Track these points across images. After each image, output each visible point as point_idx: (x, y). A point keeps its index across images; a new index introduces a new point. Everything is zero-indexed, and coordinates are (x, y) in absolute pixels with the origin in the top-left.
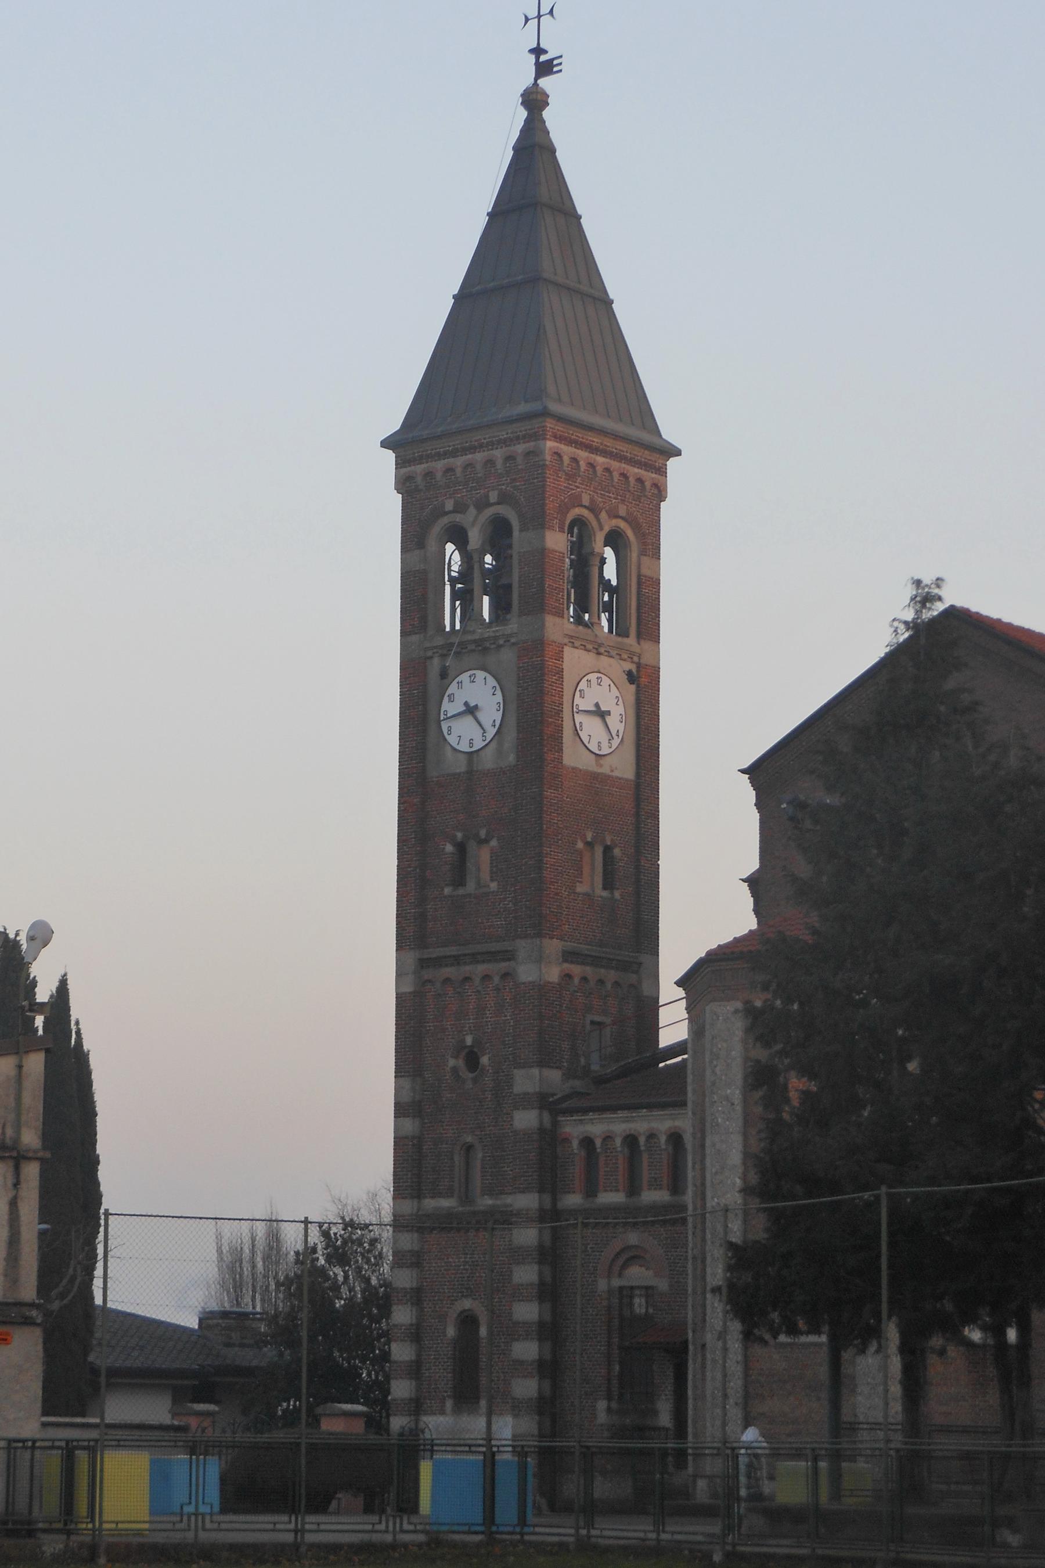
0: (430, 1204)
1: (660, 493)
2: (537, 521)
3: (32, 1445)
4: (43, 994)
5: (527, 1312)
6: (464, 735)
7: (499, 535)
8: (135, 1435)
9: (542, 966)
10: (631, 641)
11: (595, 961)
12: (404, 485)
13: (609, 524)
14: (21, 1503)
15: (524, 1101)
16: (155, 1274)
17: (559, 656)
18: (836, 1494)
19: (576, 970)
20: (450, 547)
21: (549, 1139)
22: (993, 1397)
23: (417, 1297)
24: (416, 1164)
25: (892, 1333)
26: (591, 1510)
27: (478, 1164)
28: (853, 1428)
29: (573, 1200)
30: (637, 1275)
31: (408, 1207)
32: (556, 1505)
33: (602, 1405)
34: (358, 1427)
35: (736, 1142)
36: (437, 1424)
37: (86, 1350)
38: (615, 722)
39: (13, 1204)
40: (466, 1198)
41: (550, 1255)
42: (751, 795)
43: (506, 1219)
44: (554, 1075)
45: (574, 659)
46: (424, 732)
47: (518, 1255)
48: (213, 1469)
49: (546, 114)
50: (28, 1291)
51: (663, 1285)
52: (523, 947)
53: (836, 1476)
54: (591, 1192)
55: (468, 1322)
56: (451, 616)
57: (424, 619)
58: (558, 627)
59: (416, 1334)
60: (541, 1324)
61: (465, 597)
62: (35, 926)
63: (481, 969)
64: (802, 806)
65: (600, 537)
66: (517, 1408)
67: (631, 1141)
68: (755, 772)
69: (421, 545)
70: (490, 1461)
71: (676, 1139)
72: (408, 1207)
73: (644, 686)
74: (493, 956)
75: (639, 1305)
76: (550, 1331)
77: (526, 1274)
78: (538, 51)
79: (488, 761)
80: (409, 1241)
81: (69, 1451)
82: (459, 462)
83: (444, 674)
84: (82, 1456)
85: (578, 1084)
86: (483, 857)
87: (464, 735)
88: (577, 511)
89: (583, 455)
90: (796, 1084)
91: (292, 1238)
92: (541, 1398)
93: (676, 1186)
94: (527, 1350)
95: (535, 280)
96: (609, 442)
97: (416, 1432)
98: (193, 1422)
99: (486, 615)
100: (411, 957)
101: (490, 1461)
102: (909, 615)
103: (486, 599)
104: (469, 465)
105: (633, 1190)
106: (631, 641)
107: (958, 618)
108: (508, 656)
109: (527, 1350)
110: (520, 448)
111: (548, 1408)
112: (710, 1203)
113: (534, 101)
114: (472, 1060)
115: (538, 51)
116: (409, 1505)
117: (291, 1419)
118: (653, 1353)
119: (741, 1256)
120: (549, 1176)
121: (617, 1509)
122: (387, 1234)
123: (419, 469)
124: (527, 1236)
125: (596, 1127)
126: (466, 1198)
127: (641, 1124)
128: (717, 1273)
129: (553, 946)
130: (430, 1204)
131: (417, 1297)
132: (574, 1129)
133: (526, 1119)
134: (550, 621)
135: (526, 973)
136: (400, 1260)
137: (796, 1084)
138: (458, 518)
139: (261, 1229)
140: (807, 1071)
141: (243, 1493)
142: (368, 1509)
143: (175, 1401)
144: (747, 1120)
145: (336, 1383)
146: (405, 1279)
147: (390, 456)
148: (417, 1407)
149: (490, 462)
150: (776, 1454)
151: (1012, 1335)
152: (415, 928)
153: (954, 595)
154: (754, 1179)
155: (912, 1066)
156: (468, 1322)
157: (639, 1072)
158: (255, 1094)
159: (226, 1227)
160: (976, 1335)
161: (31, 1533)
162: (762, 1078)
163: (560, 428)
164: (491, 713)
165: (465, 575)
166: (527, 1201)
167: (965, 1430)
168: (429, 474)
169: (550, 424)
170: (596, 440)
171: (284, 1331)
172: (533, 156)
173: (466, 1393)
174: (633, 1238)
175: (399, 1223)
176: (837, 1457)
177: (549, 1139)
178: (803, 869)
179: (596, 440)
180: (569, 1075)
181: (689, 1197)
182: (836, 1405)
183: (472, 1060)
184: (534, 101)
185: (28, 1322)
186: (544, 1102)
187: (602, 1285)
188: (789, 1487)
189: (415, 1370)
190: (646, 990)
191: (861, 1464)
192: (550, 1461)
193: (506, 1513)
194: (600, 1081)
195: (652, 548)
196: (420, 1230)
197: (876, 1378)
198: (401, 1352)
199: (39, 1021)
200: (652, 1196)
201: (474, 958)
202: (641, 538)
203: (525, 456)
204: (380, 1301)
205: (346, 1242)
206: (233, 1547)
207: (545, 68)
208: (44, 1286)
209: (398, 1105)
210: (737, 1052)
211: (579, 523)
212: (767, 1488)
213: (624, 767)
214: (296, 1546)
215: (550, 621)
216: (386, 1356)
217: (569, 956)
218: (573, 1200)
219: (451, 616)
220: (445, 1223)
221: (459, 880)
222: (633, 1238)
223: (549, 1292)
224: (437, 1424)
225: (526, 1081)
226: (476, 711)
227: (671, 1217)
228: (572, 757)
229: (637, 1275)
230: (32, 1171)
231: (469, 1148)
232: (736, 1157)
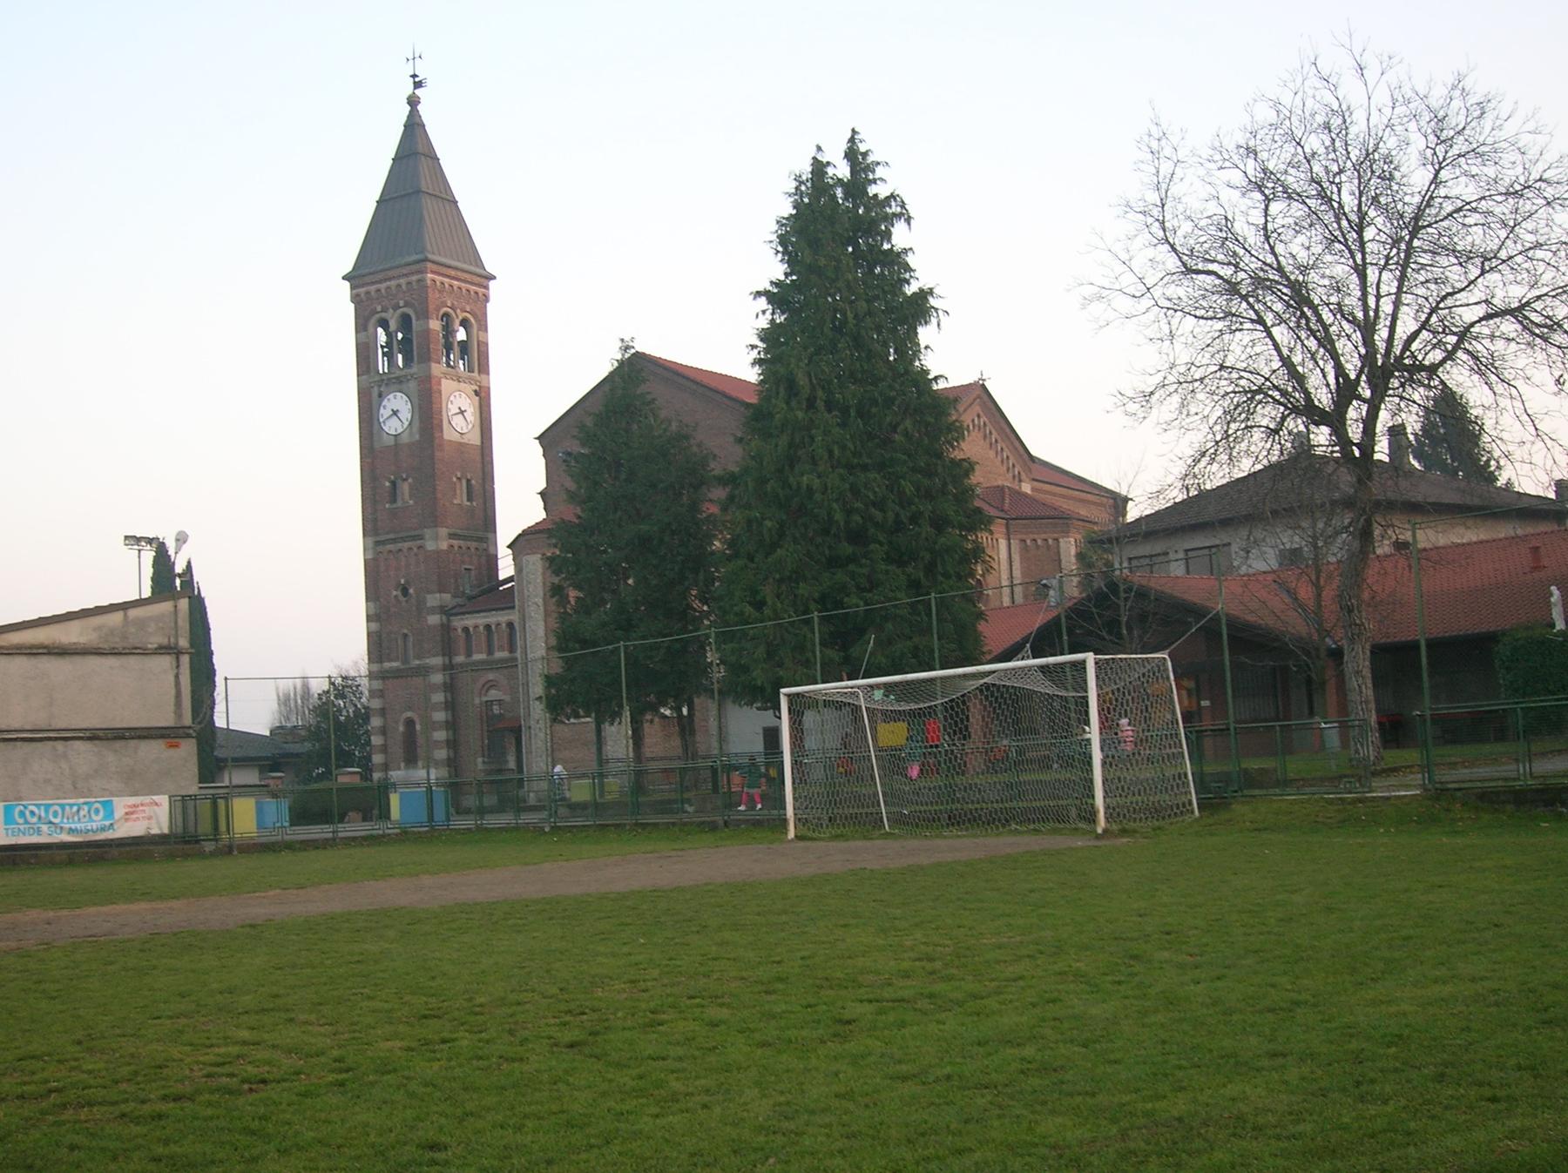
0: (387, 665)
1: (486, 298)
2: (425, 315)
3: (194, 798)
4: (179, 569)
5: (440, 716)
6: (393, 427)
7: (406, 323)
8: (244, 790)
9: (438, 541)
10: (476, 374)
11: (465, 538)
12: (355, 299)
13: (462, 315)
14: (191, 829)
15: (432, 611)
16: (247, 709)
17: (439, 384)
18: (602, 795)
19: (455, 542)
20: (380, 330)
21: (446, 628)
22: (676, 742)
23: (383, 712)
24: (378, 646)
25: (627, 714)
26: (482, 811)
27: (410, 645)
28: (607, 761)
29: (460, 659)
30: (494, 694)
31: (375, 667)
32: (462, 812)
33: (480, 760)
34: (357, 779)
35: (542, 624)
36: (396, 775)
37: (213, 749)
38: (453, 409)
39: (177, 676)
40: (405, 661)
41: (450, 687)
42: (541, 450)
43: (424, 671)
44: (447, 597)
45: (447, 385)
46: (371, 426)
47: (433, 688)
48: (285, 804)
49: (419, 107)
50: (187, 721)
51: (507, 698)
52: (428, 532)
53: (602, 785)
54: (469, 655)
55: (410, 723)
56: (382, 365)
57: (368, 367)
58: (437, 369)
59: (383, 731)
60: (447, 722)
61: (389, 356)
62: (179, 533)
63: (407, 545)
64: (569, 454)
65: (457, 322)
66: (437, 764)
67: (488, 627)
68: (540, 438)
69: (365, 329)
70: (429, 789)
71: (510, 625)
72: (375, 667)
73: (483, 397)
74: (414, 538)
75: (496, 709)
76: (452, 725)
77: (438, 697)
78: (414, 76)
79: (405, 439)
80: (377, 684)
81: (214, 800)
82: (383, 286)
83: (380, 395)
84: (221, 803)
85: (459, 600)
86: (405, 488)
87: (393, 427)
88: (445, 309)
89: (446, 280)
90: (573, 594)
91: (318, 686)
92: (449, 759)
93: (512, 649)
94: (440, 735)
95: (418, 192)
96: (459, 274)
97: (386, 779)
98: (271, 782)
99: (400, 363)
100: (370, 540)
101: (429, 789)
102: (619, 357)
103: (400, 356)
104: (388, 288)
105: (490, 652)
106: (476, 374)
107: (639, 356)
108: (412, 385)
109: (440, 735)
110: (414, 278)
111: (453, 763)
112: (530, 656)
113: (413, 102)
114: (405, 591)
115: (414, 76)
116: (385, 814)
117: (321, 777)
118: (505, 732)
119: (549, 681)
120: (448, 649)
121: (492, 810)
122: (365, 682)
123: (362, 290)
124: (437, 678)
125: (469, 621)
126: (405, 661)
127: (493, 618)
128: (538, 689)
129: (443, 531)
130: (387, 665)
131: (383, 712)
132: (459, 623)
133: (434, 620)
134: (434, 365)
135: (430, 546)
136: (373, 693)
137: (573, 594)
138: (383, 315)
139: (299, 683)
140: (578, 587)
141: (301, 816)
142: (364, 820)
143: (261, 772)
144: (547, 614)
145: (345, 759)
146: (376, 704)
147: (347, 284)
148: (386, 767)
149: (399, 286)
150: (571, 777)
151: (685, 711)
152: (371, 526)
153: (640, 347)
154: (553, 642)
155: (630, 581)
156: (410, 723)
157: (490, 593)
158: (295, 617)
159: (281, 683)
160: (668, 713)
161: (197, 842)
162: (556, 591)
163: (435, 267)
164: (406, 413)
165: (389, 344)
166: (437, 661)
167: (662, 759)
168: (368, 293)
169: (429, 265)
170: (453, 273)
171: (315, 734)
172: (414, 128)
173: (411, 760)
174: (491, 676)
175: (371, 676)
176: (602, 776)
177: (446, 628)
178: (570, 485)
179: (453, 273)
180: (454, 597)
181: (518, 654)
182: (600, 750)
183: (405, 591)
184: (413, 102)
185: (189, 736)
186: (443, 610)
187: (477, 701)
188: (580, 792)
189: (384, 749)
190: (492, 551)
191: (611, 779)
192: (455, 788)
193: (440, 814)
194: (470, 598)
195: (483, 326)
196: (383, 678)
197: (618, 738)
198: (376, 740)
199: (178, 582)
200: (499, 655)
201: (403, 539)
202: (477, 320)
203: (414, 279)
204: (364, 716)
205: (342, 688)
206: (302, 842)
207: (418, 85)
208: (194, 719)
209: (368, 616)
210: (540, 580)
211: (446, 315)
212: (568, 795)
213: (475, 439)
214: (334, 839)
215: (434, 365)
216: (368, 743)
217: (452, 536)
218: (460, 659)
219: (382, 365)
220: (397, 674)
221: (394, 501)
222: (491, 676)
223: (450, 706)
224: (396, 775)
225: (433, 600)
226: (397, 413)
227: (510, 664)
228: (448, 435)
229: (494, 694)
230: (185, 659)
231: (405, 635)
232: (541, 632)
